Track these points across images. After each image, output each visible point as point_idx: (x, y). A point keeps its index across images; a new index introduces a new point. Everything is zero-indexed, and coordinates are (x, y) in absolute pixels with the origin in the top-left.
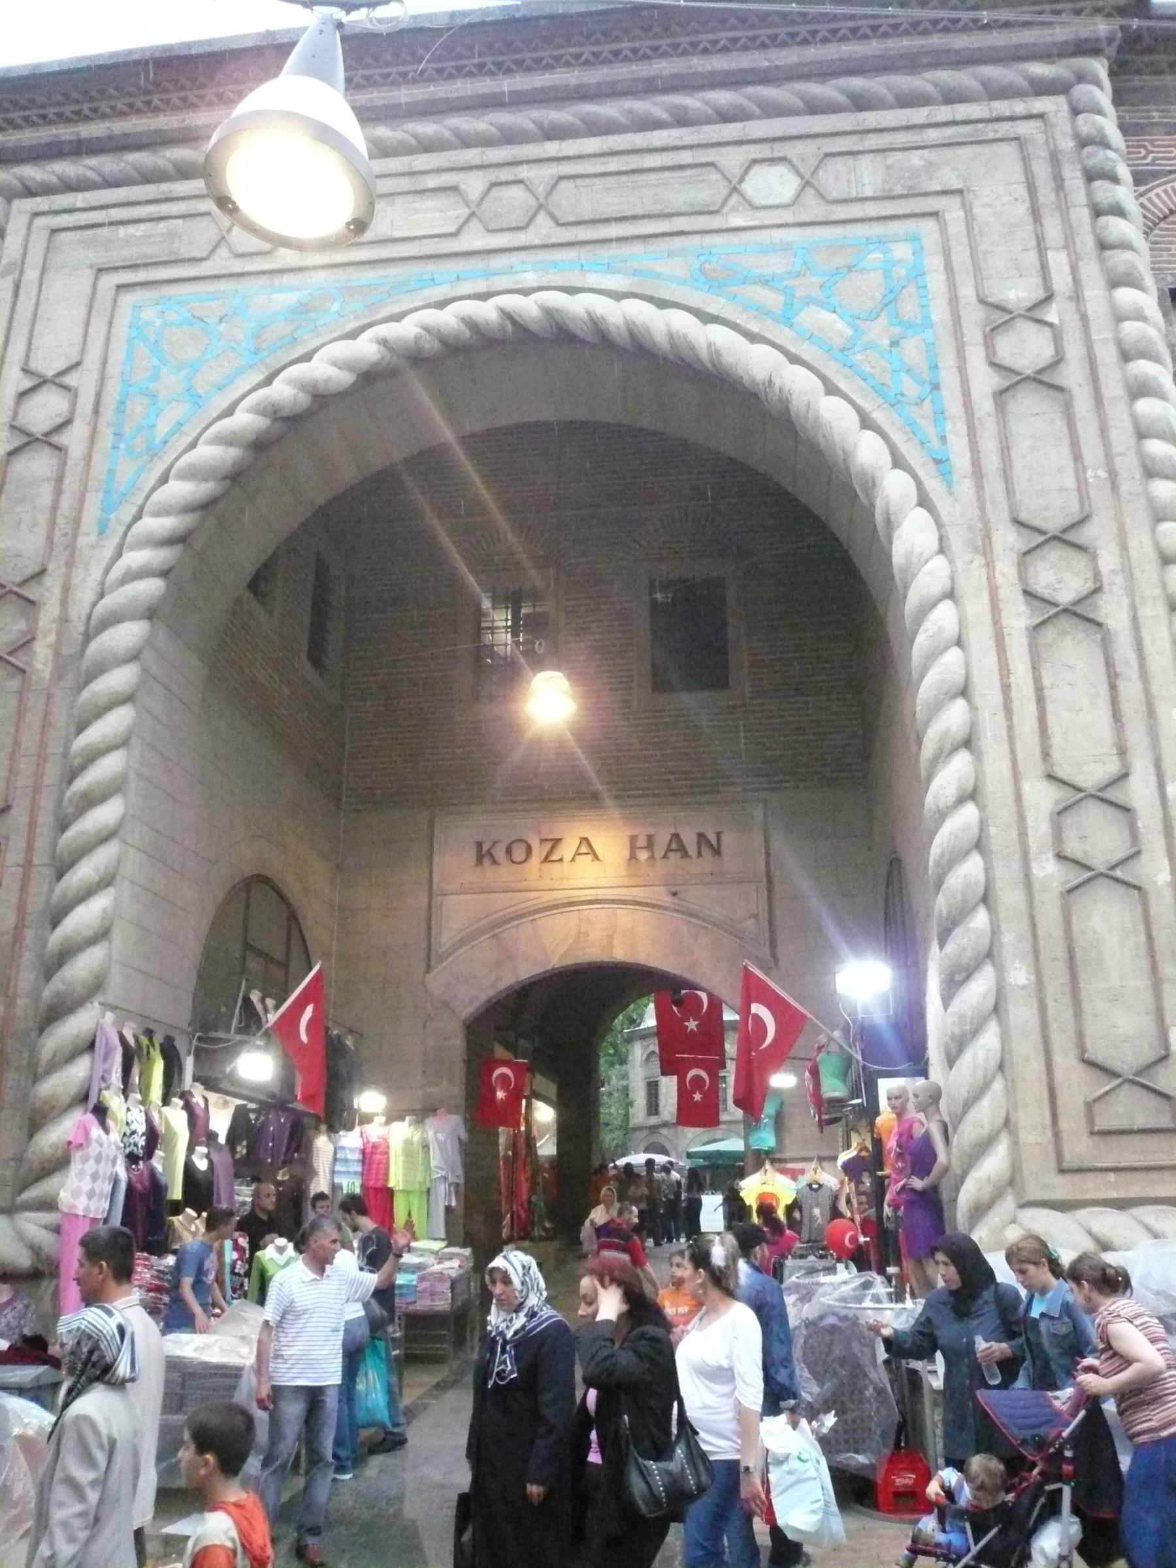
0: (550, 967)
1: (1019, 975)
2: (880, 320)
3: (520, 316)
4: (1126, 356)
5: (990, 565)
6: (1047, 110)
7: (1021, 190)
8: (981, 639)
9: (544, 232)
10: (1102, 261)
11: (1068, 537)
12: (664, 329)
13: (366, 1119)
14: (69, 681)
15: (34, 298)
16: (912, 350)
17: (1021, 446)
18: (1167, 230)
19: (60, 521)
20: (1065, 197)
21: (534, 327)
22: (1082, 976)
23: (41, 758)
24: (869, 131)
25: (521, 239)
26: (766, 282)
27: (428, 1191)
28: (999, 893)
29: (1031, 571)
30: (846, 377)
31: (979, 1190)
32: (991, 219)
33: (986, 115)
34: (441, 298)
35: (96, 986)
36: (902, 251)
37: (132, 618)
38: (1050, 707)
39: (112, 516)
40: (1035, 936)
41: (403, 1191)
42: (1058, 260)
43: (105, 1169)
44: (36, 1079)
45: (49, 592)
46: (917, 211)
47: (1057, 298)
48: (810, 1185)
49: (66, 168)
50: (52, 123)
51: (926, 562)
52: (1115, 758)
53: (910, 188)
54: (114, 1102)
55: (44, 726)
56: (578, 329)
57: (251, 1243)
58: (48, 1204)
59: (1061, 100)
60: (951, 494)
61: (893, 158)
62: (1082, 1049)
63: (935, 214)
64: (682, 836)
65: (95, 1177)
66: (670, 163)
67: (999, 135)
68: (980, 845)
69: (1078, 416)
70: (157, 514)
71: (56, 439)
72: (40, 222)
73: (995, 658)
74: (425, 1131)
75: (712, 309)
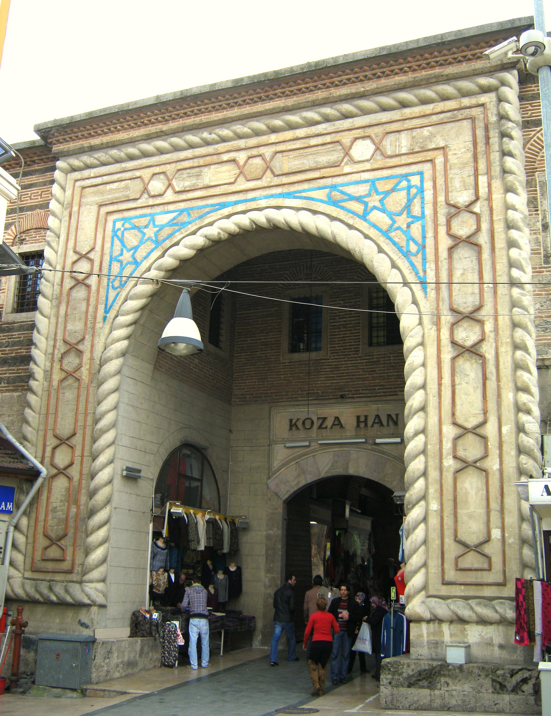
0: (321, 477)
1: (434, 506)
2: (403, 216)
5: (439, 330)
6: (486, 101)
9: (269, 180)
10: (503, 179)
16: (416, 230)
19: (89, 317)
20: (490, 147)
23: (86, 414)
26: (358, 199)
28: (429, 472)
29: (455, 332)
30: (387, 244)
33: (457, 107)
36: (415, 180)
39: (108, 315)
42: (483, 180)
44: (87, 536)
45: (85, 347)
47: (481, 200)
49: (87, 159)
50: (80, 139)
52: (482, 415)
53: (422, 147)
56: (282, 226)
59: (493, 95)
60: (426, 297)
61: (415, 133)
62: (456, 536)
63: (431, 161)
67: (463, 117)
68: (424, 452)
72: (78, 184)
75: (334, 214)
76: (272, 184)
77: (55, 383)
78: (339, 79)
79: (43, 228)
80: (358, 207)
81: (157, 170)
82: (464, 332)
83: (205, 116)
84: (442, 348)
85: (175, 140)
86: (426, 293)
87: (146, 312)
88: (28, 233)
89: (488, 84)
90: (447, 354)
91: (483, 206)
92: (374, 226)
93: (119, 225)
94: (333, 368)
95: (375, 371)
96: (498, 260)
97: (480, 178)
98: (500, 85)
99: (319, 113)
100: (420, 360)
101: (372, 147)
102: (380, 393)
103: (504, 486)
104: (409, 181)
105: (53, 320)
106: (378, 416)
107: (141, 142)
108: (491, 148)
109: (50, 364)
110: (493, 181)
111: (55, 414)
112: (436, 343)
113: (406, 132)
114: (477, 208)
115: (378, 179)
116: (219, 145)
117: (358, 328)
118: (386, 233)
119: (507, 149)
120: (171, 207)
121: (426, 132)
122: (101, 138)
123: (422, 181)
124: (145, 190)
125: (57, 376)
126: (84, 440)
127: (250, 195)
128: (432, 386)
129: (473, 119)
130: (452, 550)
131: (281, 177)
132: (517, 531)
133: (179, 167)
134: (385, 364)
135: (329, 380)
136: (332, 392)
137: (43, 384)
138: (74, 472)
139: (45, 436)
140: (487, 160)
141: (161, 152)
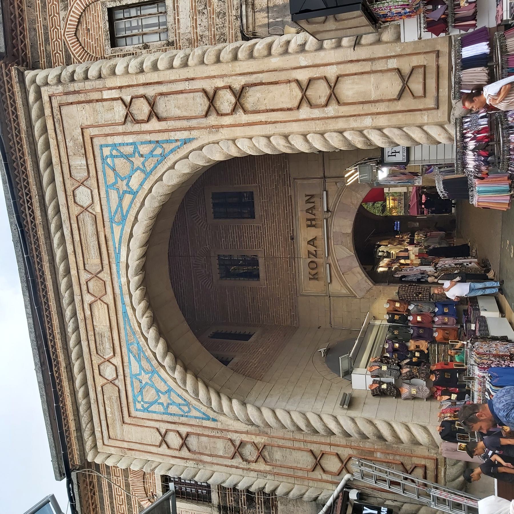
1: (368, 121)
4: (142, 71)
5: (222, 126)
6: (48, 95)
14: (268, 430)
16: (144, 149)
18: (88, 47)
19: (213, 434)
23: (294, 440)
26: (121, 199)
28: (339, 128)
36: (107, 151)
39: (211, 417)
40: (355, 116)
42: (106, 95)
45: (237, 438)
59: (43, 89)
60: (197, 139)
61: (70, 153)
67: (59, 113)
71: (184, 436)
72: (106, 442)
73: (258, 87)
75: (133, 219)
76: (109, 272)
77: (268, 468)
78: (28, 216)
79: (144, 475)
80: (128, 198)
81: (96, 371)
83: (55, 331)
84: (237, 123)
85: (73, 356)
87: (211, 383)
88: (147, 489)
89: (34, 93)
90: (241, 117)
92: (141, 185)
93: (139, 406)
94: (271, 246)
95: (273, 213)
96: (167, 79)
97: (105, 97)
98: (35, 84)
99: (55, 234)
100: (246, 142)
101: (82, 188)
104: (107, 157)
105: (215, 468)
106: (307, 211)
107: (75, 386)
108: (82, 89)
109: (252, 472)
110: (107, 86)
112: (233, 128)
113: (70, 161)
114: (128, 99)
115: (106, 183)
116: (79, 318)
117: (241, 227)
118: (148, 175)
120: (126, 359)
121: (70, 144)
122: (70, 421)
123: (107, 146)
124: (112, 382)
125: (261, 466)
126: (316, 443)
127: (117, 291)
128: (268, 129)
129: (60, 106)
130: (408, 102)
131: (103, 265)
132: (389, 45)
133: (95, 352)
134: (268, 206)
135: (280, 250)
136: (289, 247)
137: (269, 480)
138: (345, 453)
139: (313, 480)
140: (91, 92)
141: (83, 369)
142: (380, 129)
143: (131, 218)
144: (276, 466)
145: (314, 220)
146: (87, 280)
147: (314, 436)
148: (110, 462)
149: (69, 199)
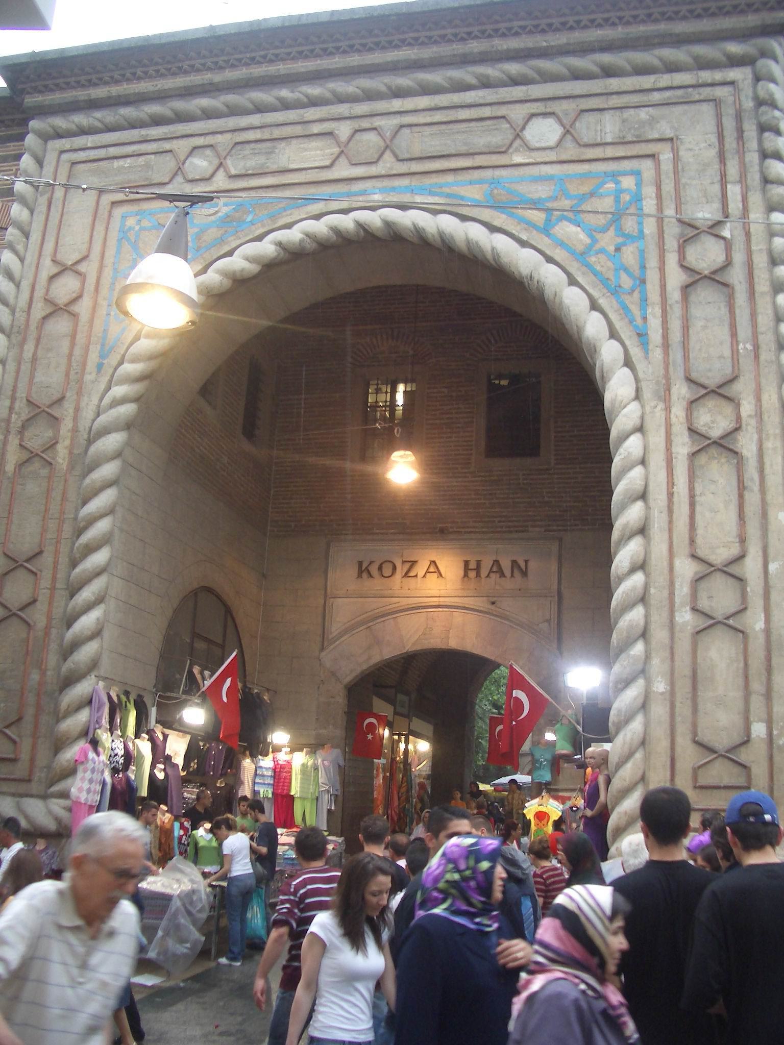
1: (660, 686)
3: (369, 226)
5: (668, 409)
7: (714, 139)
8: (657, 460)
9: (388, 165)
10: (764, 191)
11: (721, 391)
12: (463, 237)
13: (277, 749)
14: (77, 472)
15: (60, 210)
16: (629, 255)
17: (697, 326)
19: (74, 364)
20: (743, 144)
21: (379, 234)
22: (700, 687)
23: (61, 521)
24: (612, 94)
25: (373, 170)
26: (535, 204)
27: (317, 799)
29: (695, 414)
30: (583, 274)
31: (620, 818)
32: (691, 160)
33: (693, 82)
34: (318, 213)
35: (94, 665)
36: (628, 182)
37: (117, 430)
38: (698, 508)
39: (105, 362)
41: (300, 798)
42: (734, 191)
43: (97, 777)
45: (66, 412)
46: (641, 153)
48: (571, 808)
49: (81, 119)
50: (73, 88)
51: (625, 407)
52: (737, 544)
53: (637, 136)
54: (105, 737)
55: (62, 500)
57: (192, 825)
58: (65, 795)
60: (647, 358)
61: (628, 114)
62: (695, 733)
63: (652, 156)
64: (501, 563)
65: (91, 781)
66: (475, 116)
67: (702, 97)
68: (643, 599)
69: (737, 305)
70: (132, 361)
72: (65, 157)
74: (316, 759)
75: (497, 223)
78: (508, 25)
80: (538, 217)
81: (200, 141)
82: (709, 415)
84: (673, 437)
86: (646, 351)
90: (683, 447)
91: (736, 228)
92: (561, 244)
102: (501, 527)
103: (773, 655)
104: (617, 183)
110: (749, 194)
111: (8, 518)
119: (772, 148)
121: (643, 114)
123: (639, 184)
128: (658, 496)
129: (716, 102)
138: (38, 615)
142: (644, 706)
143: (499, 220)
144: (13, 483)
145: (478, 575)
146: (379, 130)
147: (67, 559)
148: (26, 161)
149: (539, 104)
